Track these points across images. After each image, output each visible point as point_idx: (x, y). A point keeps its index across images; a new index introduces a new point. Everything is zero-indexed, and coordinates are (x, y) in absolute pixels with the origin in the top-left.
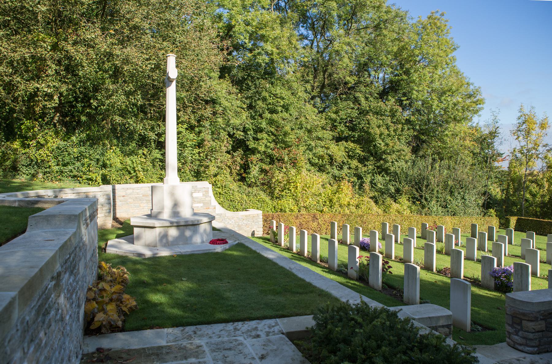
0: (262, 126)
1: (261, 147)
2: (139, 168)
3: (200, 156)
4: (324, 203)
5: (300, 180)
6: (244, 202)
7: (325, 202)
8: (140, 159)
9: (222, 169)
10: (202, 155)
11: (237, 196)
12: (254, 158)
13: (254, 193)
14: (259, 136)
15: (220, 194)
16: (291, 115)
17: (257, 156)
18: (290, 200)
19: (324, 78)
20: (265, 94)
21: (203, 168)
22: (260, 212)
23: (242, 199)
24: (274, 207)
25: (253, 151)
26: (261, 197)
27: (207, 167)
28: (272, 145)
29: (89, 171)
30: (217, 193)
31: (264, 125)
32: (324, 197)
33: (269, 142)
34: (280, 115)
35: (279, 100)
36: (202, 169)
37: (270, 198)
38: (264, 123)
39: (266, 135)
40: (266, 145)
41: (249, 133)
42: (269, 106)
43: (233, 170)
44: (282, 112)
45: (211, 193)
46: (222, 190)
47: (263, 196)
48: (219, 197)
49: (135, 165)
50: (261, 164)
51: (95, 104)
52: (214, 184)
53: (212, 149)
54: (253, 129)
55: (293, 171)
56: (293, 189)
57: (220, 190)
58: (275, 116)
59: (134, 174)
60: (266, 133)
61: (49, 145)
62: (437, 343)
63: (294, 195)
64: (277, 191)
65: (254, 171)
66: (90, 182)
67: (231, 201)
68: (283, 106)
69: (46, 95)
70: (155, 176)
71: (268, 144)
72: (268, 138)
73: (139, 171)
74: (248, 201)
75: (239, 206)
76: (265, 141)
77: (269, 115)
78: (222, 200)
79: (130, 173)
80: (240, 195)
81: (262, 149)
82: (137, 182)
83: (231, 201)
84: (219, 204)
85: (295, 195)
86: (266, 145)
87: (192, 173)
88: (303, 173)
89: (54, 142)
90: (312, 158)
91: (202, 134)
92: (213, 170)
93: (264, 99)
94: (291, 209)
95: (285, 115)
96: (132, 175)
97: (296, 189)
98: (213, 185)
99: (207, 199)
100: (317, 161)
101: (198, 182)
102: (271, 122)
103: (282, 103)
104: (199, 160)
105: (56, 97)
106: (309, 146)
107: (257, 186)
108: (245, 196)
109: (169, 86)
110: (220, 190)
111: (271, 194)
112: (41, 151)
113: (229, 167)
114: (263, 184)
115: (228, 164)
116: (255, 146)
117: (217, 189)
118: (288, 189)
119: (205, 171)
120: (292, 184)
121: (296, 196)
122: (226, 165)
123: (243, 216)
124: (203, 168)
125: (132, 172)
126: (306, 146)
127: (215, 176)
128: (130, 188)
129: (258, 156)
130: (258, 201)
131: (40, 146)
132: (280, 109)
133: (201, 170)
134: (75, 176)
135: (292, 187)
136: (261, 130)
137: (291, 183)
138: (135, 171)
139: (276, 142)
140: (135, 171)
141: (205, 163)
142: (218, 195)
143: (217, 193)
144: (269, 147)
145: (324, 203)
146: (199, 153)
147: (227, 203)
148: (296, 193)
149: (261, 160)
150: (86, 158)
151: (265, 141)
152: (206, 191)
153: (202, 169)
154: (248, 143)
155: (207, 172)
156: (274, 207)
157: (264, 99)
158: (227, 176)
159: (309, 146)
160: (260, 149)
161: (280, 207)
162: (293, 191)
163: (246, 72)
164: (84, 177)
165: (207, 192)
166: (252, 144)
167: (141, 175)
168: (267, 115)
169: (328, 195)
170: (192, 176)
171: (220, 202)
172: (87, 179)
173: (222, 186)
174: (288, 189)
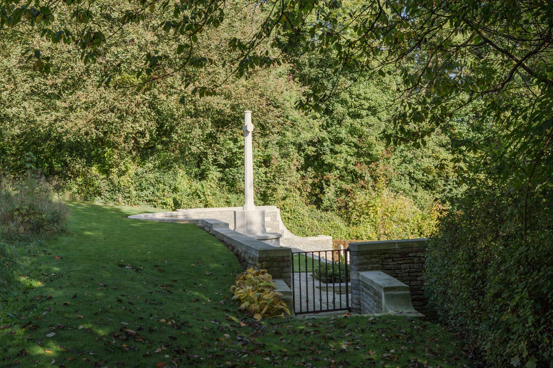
0: (341, 135)
1: (339, 162)
2: (208, 192)
3: (266, 177)
4: (412, 231)
5: (380, 204)
6: (315, 228)
7: (414, 230)
8: (209, 183)
9: (291, 192)
10: (268, 175)
11: (307, 221)
12: (332, 176)
13: (326, 218)
14: (337, 148)
15: (289, 218)
16: (379, 119)
17: (335, 173)
18: (368, 226)
19: (430, 61)
20: (345, 95)
21: (270, 190)
22: (331, 238)
23: (313, 224)
24: (349, 234)
25: (330, 167)
26: (335, 222)
27: (275, 190)
28: (353, 160)
29: (164, 196)
30: (285, 218)
31: (343, 133)
32: (413, 223)
33: (351, 155)
34: (365, 120)
35: (363, 102)
36: (269, 192)
37: (346, 224)
38: (344, 131)
39: (346, 147)
40: (346, 160)
41: (325, 144)
42: (351, 110)
43: (303, 193)
44: (367, 115)
45: (279, 218)
46: (291, 215)
47: (338, 221)
48: (288, 222)
49: (205, 190)
50: (341, 182)
51: (176, 137)
52: (282, 208)
53: (280, 169)
54: (330, 139)
55: (374, 194)
56: (373, 214)
57: (289, 215)
58: (357, 123)
59: (203, 198)
60: (347, 144)
61: (130, 171)
62: (333, 259)
63: (373, 221)
64: (354, 216)
65: (330, 193)
66: (164, 206)
67: (301, 226)
68: (369, 109)
69: (138, 132)
70: (222, 200)
71: (349, 158)
72: (348, 150)
73: (209, 195)
74: (319, 228)
75: (309, 232)
76: (344, 155)
77: (351, 121)
78: (290, 225)
79: (200, 197)
80: (311, 220)
81: (340, 164)
82: (206, 206)
83: (301, 226)
84: (288, 229)
85: (374, 220)
86: (346, 160)
87: (259, 195)
88: (385, 196)
89: (133, 169)
90: (414, 173)
91: (269, 150)
92: (281, 192)
93: (343, 102)
94: (369, 237)
95: (372, 119)
96: (202, 199)
97: (377, 214)
98: (281, 209)
99: (275, 223)
100: (420, 176)
101: (266, 206)
102: (353, 131)
103: (367, 105)
104: (265, 181)
105: (148, 136)
106: (405, 157)
107: (334, 210)
108: (316, 222)
109: (247, 136)
110: (289, 215)
111: (348, 220)
112: (122, 178)
113: (299, 189)
114: (340, 208)
115: (298, 186)
116: (331, 161)
117: (285, 214)
118: (367, 214)
119: (273, 195)
120: (371, 208)
121: (375, 222)
122: (296, 187)
123: (312, 241)
124: (270, 190)
125: (202, 196)
126: (401, 158)
127: (284, 199)
128: (203, 212)
129: (337, 172)
130: (332, 227)
131: (122, 173)
132: (364, 113)
133: (268, 192)
134: (150, 201)
135: (371, 211)
136: (339, 141)
137: (370, 207)
138: (205, 195)
139: (358, 155)
140: (205, 195)
141: (271, 185)
142: (286, 220)
143: (285, 218)
144: (350, 162)
145: (412, 231)
146: (266, 173)
147: (296, 229)
148: (375, 219)
149: (341, 178)
150: (161, 183)
151: (344, 155)
152: (274, 216)
153: (269, 192)
154: (324, 157)
155: (275, 196)
156: (349, 234)
157: (343, 102)
158: (297, 199)
159: (405, 157)
160: (337, 164)
161: (355, 234)
162: (372, 216)
163: (320, 70)
164: (160, 201)
165: (275, 216)
166: (328, 159)
167: (210, 199)
168: (348, 120)
169: (418, 221)
170: (259, 199)
171: (289, 228)
172: (162, 203)
173: (291, 210)
174: (367, 214)
